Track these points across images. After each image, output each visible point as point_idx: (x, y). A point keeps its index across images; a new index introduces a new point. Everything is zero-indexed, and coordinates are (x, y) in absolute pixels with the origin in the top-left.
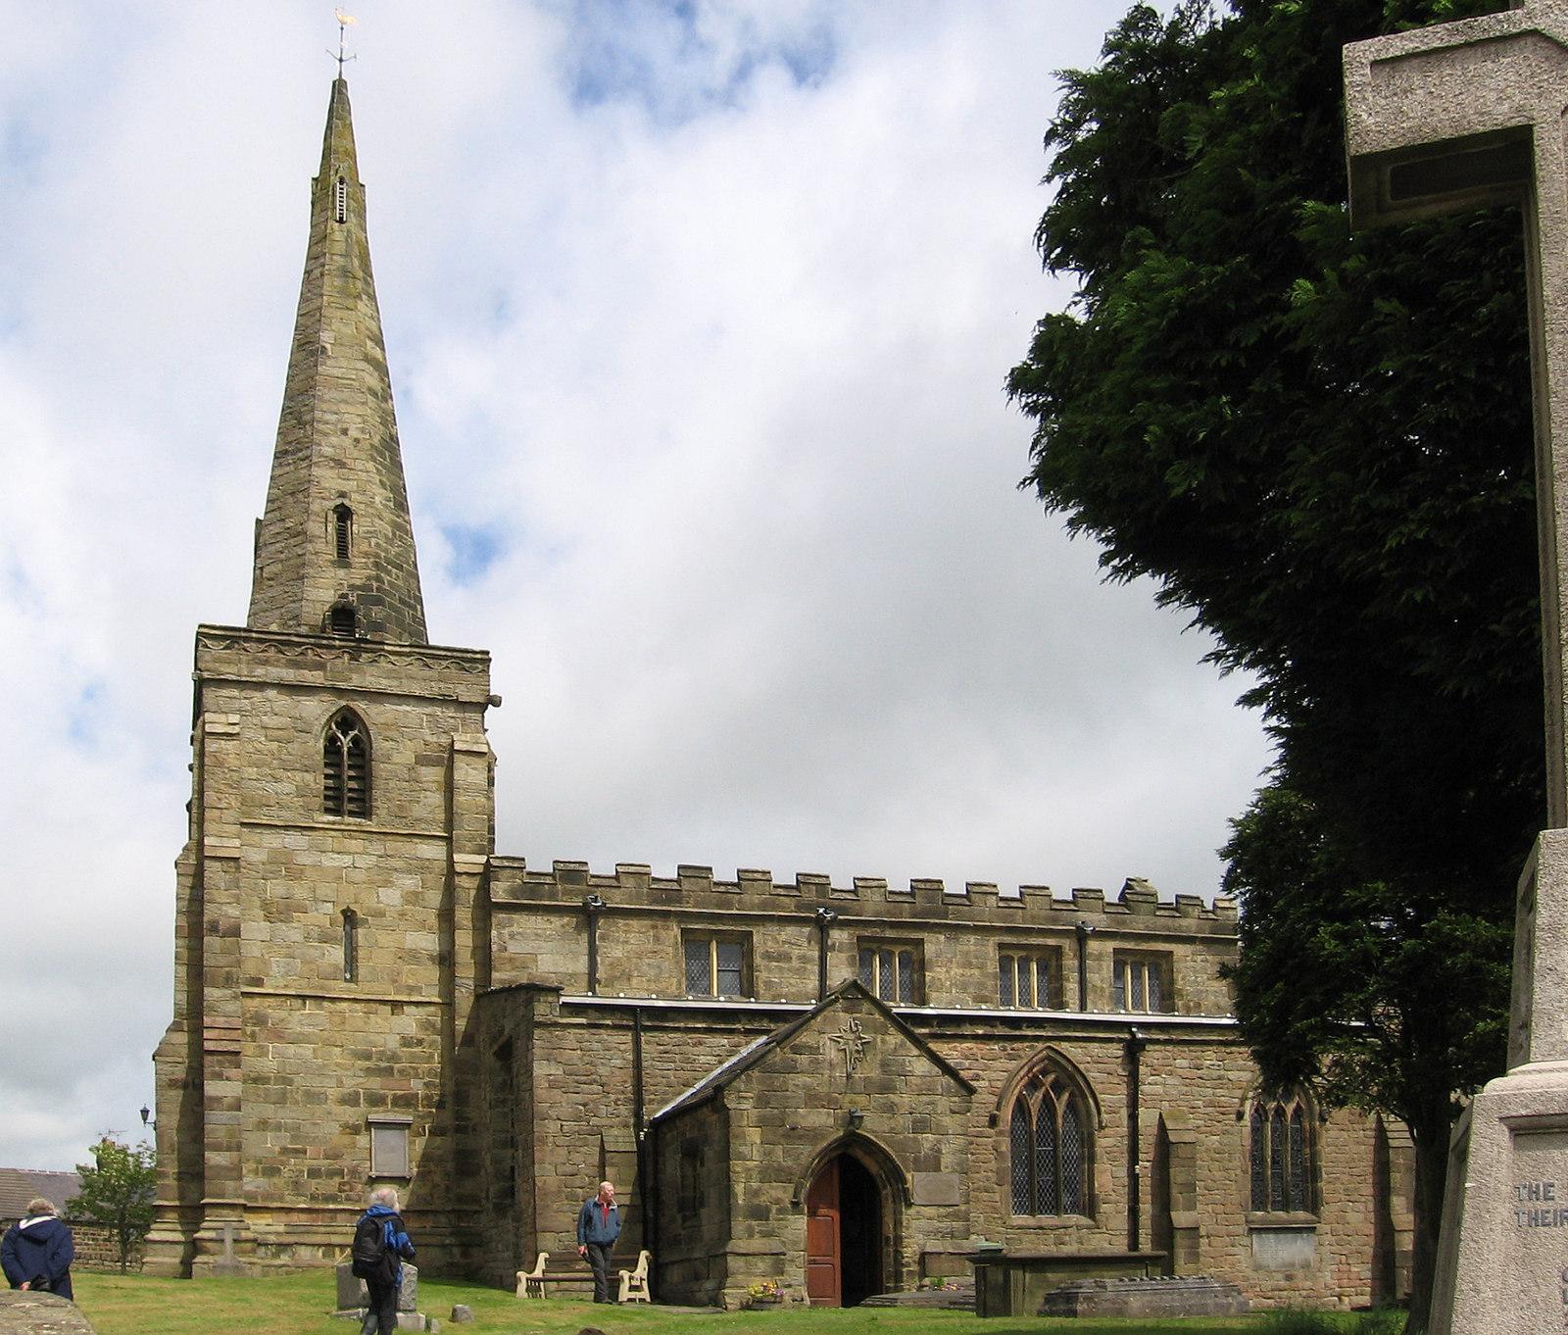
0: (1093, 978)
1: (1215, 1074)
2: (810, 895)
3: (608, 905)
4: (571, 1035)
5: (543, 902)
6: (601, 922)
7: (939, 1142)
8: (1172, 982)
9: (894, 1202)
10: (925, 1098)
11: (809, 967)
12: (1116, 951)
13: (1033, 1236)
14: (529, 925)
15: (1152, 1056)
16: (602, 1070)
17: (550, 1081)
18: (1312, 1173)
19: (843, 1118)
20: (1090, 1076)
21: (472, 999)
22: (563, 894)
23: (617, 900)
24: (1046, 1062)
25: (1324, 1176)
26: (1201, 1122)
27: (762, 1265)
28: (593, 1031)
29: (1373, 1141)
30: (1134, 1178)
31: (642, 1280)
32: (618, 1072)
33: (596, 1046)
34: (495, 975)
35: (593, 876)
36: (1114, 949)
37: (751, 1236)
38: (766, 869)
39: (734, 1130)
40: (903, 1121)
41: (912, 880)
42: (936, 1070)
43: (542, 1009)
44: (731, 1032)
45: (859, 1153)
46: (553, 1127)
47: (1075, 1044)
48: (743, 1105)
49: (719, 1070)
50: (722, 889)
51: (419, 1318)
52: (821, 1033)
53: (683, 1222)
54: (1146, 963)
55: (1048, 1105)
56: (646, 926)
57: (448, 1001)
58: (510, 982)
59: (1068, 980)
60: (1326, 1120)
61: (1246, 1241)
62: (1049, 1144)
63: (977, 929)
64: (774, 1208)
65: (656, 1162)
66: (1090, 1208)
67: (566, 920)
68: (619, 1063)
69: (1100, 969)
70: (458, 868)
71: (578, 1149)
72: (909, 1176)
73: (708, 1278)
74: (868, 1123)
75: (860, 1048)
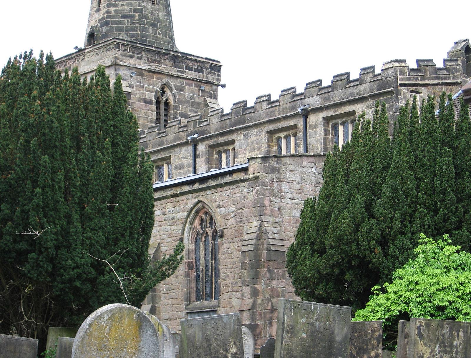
54: (349, 121)
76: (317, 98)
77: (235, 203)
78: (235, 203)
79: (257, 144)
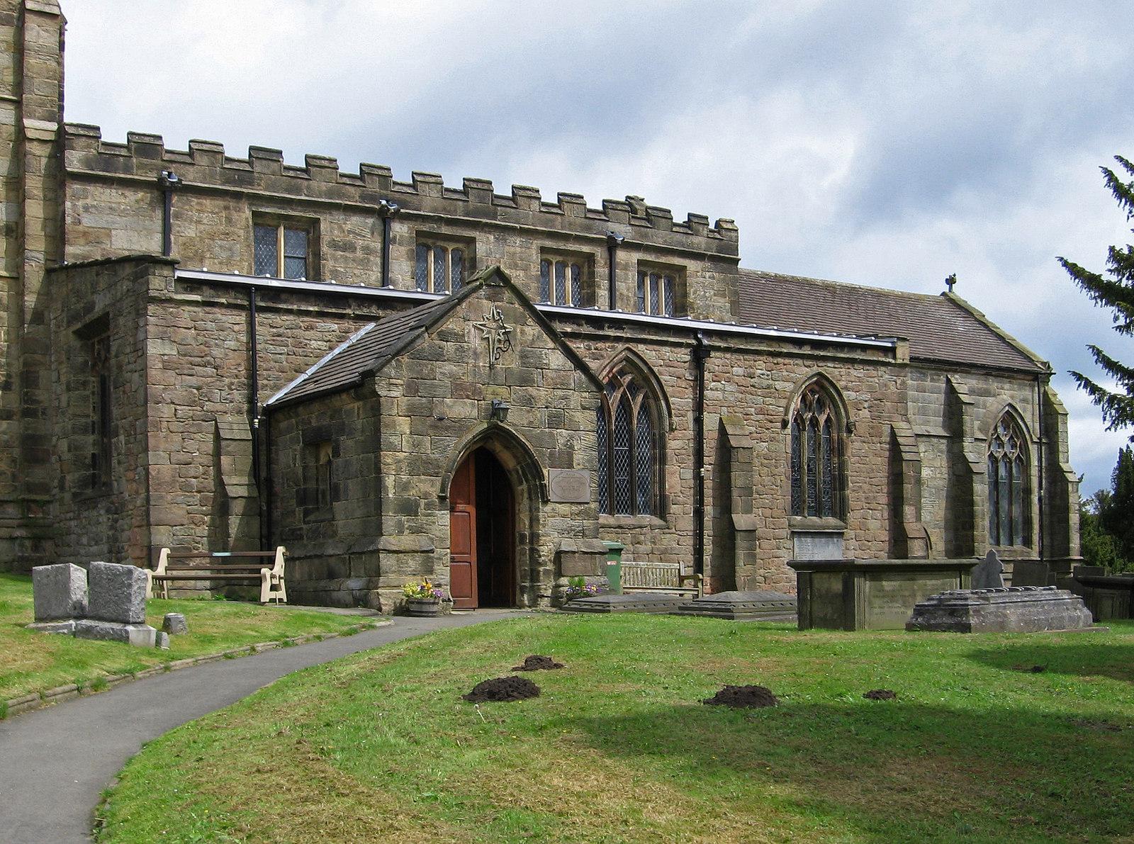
0: (621, 286)
1: (765, 383)
2: (373, 186)
3: (183, 183)
4: (186, 313)
5: (118, 175)
6: (175, 199)
7: (572, 437)
8: (685, 295)
9: (530, 499)
10: (560, 393)
11: (372, 258)
12: (640, 262)
13: (614, 535)
14: (103, 197)
15: (715, 362)
16: (216, 352)
17: (163, 362)
18: (839, 481)
19: (487, 409)
20: (663, 378)
21: (42, 273)
22: (138, 168)
23: (191, 177)
24: (624, 363)
25: (850, 485)
26: (753, 429)
27: (413, 563)
28: (207, 309)
29: (887, 454)
30: (699, 479)
31: (280, 578)
32: (231, 354)
33: (210, 325)
34: (69, 249)
35: (167, 152)
36: (638, 260)
37: (401, 532)
38: (332, 157)
39: (385, 419)
40: (541, 415)
41: (464, 179)
42: (570, 364)
43: (158, 283)
44: (342, 316)
45: (498, 447)
46: (166, 411)
47: (650, 347)
48: (392, 391)
49: (329, 357)
50: (291, 173)
51: (149, 631)
52: (465, 320)
53: (304, 517)
54: (663, 276)
55: (625, 404)
56: (218, 206)
57: (14, 275)
58: (84, 257)
59: (599, 287)
60: (851, 432)
61: (788, 544)
62: (625, 445)
63: (522, 232)
64: (423, 502)
65: (269, 451)
66: (661, 509)
67: (140, 195)
68: (232, 344)
69: (626, 279)
70: (29, 134)
71: (192, 436)
72: (545, 472)
73: (349, 576)
74: (511, 417)
75: (502, 337)
76: (628, 228)
77: (871, 390)
78: (871, 390)
79: (522, 260)
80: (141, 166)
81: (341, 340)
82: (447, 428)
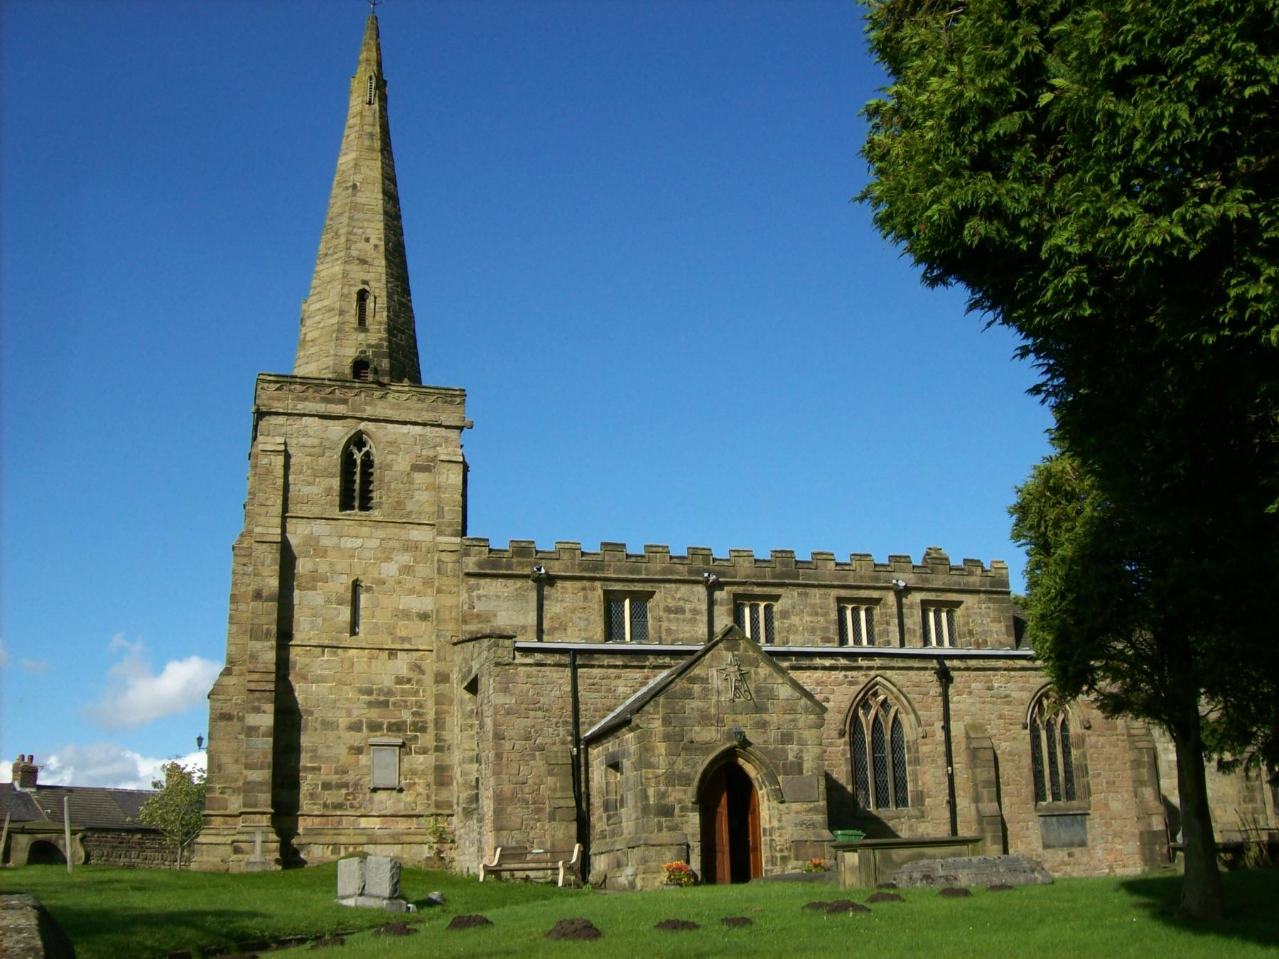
0: (908, 623)
2: (699, 564)
7: (801, 751)
10: (789, 717)
23: (557, 569)
37: (660, 830)
40: (773, 735)
42: (797, 695)
44: (643, 667)
69: (912, 615)
80: (520, 564)
81: (643, 684)
82: (696, 749)
